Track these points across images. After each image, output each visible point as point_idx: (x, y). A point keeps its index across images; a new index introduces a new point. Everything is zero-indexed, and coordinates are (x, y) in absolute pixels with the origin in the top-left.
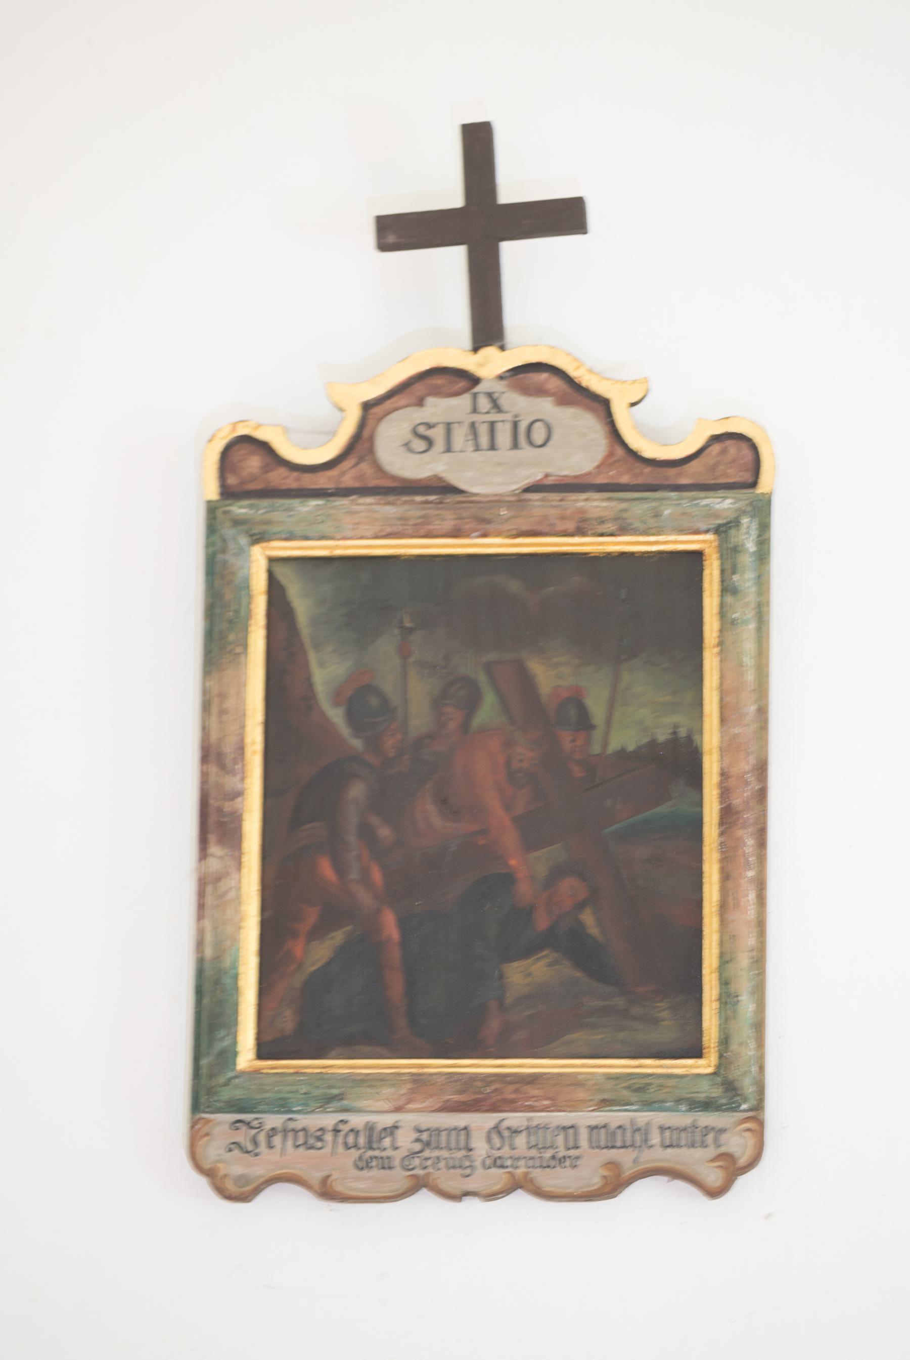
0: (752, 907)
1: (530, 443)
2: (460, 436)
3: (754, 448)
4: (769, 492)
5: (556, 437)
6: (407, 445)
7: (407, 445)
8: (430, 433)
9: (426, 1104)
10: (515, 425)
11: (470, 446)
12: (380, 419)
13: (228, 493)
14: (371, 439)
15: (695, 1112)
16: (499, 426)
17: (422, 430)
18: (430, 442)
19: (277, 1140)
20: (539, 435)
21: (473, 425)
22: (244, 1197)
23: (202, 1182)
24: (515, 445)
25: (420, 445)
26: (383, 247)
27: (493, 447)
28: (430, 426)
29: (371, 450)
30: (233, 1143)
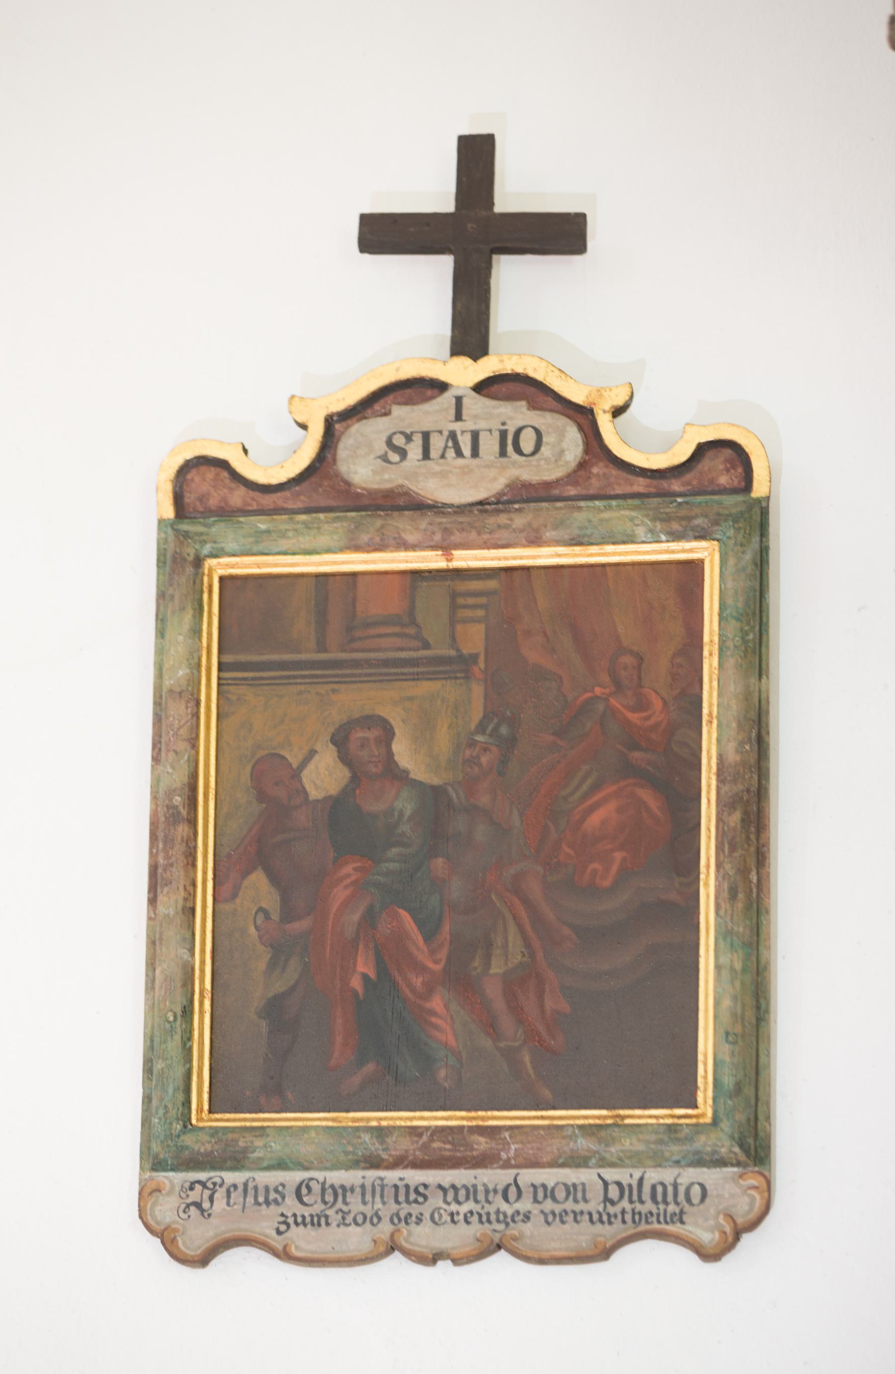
1: (518, 450)
2: (437, 443)
7: (385, 458)
11: (451, 453)
16: (483, 438)
20: (527, 442)
21: (453, 436)
22: (203, 1260)
24: (503, 453)
27: (475, 453)
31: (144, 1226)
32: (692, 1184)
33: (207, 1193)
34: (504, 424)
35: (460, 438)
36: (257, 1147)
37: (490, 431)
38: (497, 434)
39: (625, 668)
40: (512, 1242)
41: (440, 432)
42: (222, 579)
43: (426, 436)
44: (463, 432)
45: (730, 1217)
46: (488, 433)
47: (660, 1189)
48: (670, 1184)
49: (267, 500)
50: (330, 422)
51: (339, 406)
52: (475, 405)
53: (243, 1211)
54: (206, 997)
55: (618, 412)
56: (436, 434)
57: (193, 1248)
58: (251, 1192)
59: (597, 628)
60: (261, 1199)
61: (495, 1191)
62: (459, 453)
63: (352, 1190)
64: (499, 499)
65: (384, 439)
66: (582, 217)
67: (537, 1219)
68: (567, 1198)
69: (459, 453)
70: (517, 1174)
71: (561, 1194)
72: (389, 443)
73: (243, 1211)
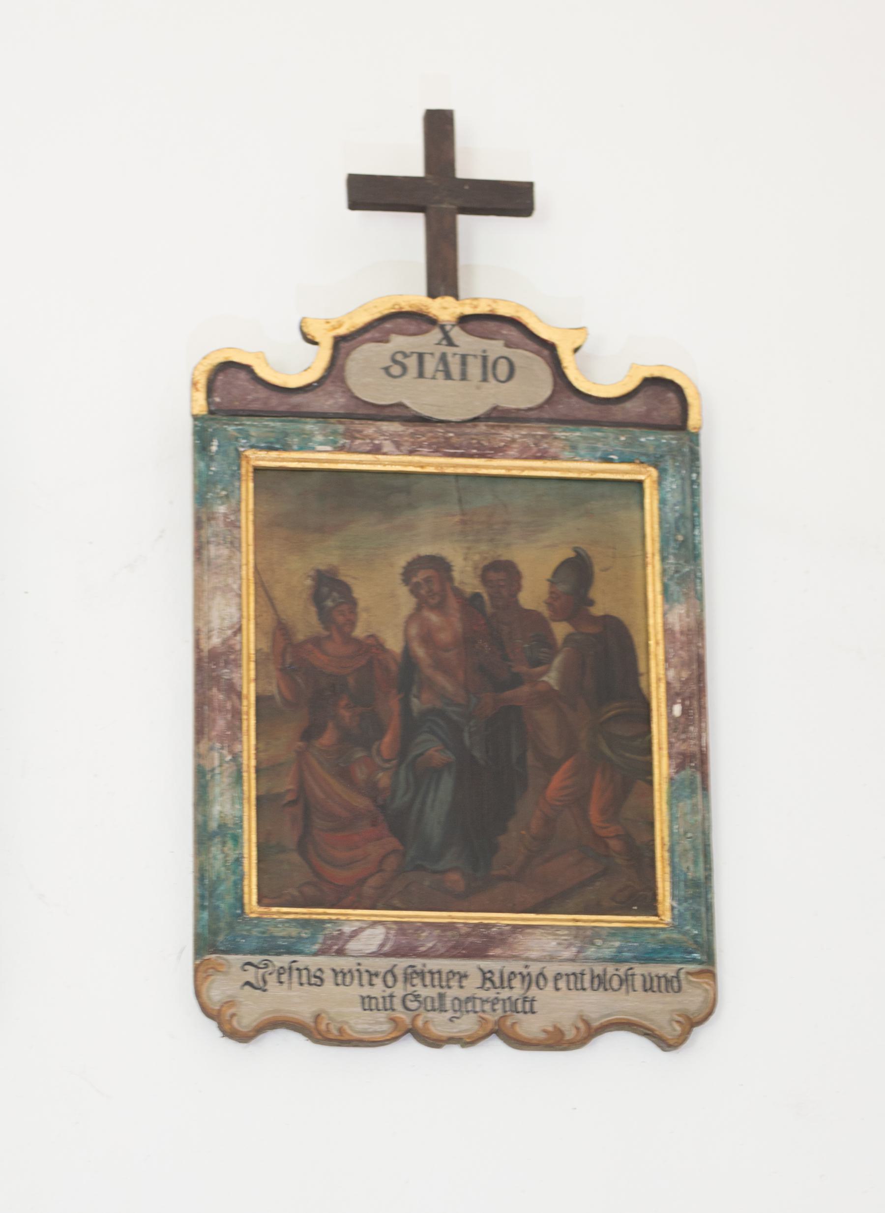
0: (665, 784)
1: (495, 376)
2: (430, 365)
3: (678, 390)
4: (698, 426)
5: (518, 372)
6: (387, 369)
7: (387, 369)
8: (406, 361)
9: (417, 952)
10: (485, 359)
11: (440, 375)
12: (348, 354)
13: (213, 412)
14: (342, 369)
15: (581, 962)
16: (470, 360)
17: (399, 357)
18: (404, 368)
19: (562, 984)
21: (443, 358)
23: (212, 1025)
25: (396, 370)
26: (354, 204)
27: (464, 377)
28: (405, 355)
29: (342, 380)
30: (541, 989)
32: (428, 997)
34: (484, 351)
35: (450, 359)
36: (671, 609)
41: (432, 354)
45: (586, 1022)
48: (393, 992)
50: (339, 341)
51: (343, 331)
52: (456, 334)
53: (316, 343)
54: (445, 993)
55: (576, 350)
56: (430, 356)
57: (246, 1020)
59: (464, 952)
60: (436, 976)
62: (448, 376)
63: (376, 975)
71: (328, 975)
73: (316, 343)
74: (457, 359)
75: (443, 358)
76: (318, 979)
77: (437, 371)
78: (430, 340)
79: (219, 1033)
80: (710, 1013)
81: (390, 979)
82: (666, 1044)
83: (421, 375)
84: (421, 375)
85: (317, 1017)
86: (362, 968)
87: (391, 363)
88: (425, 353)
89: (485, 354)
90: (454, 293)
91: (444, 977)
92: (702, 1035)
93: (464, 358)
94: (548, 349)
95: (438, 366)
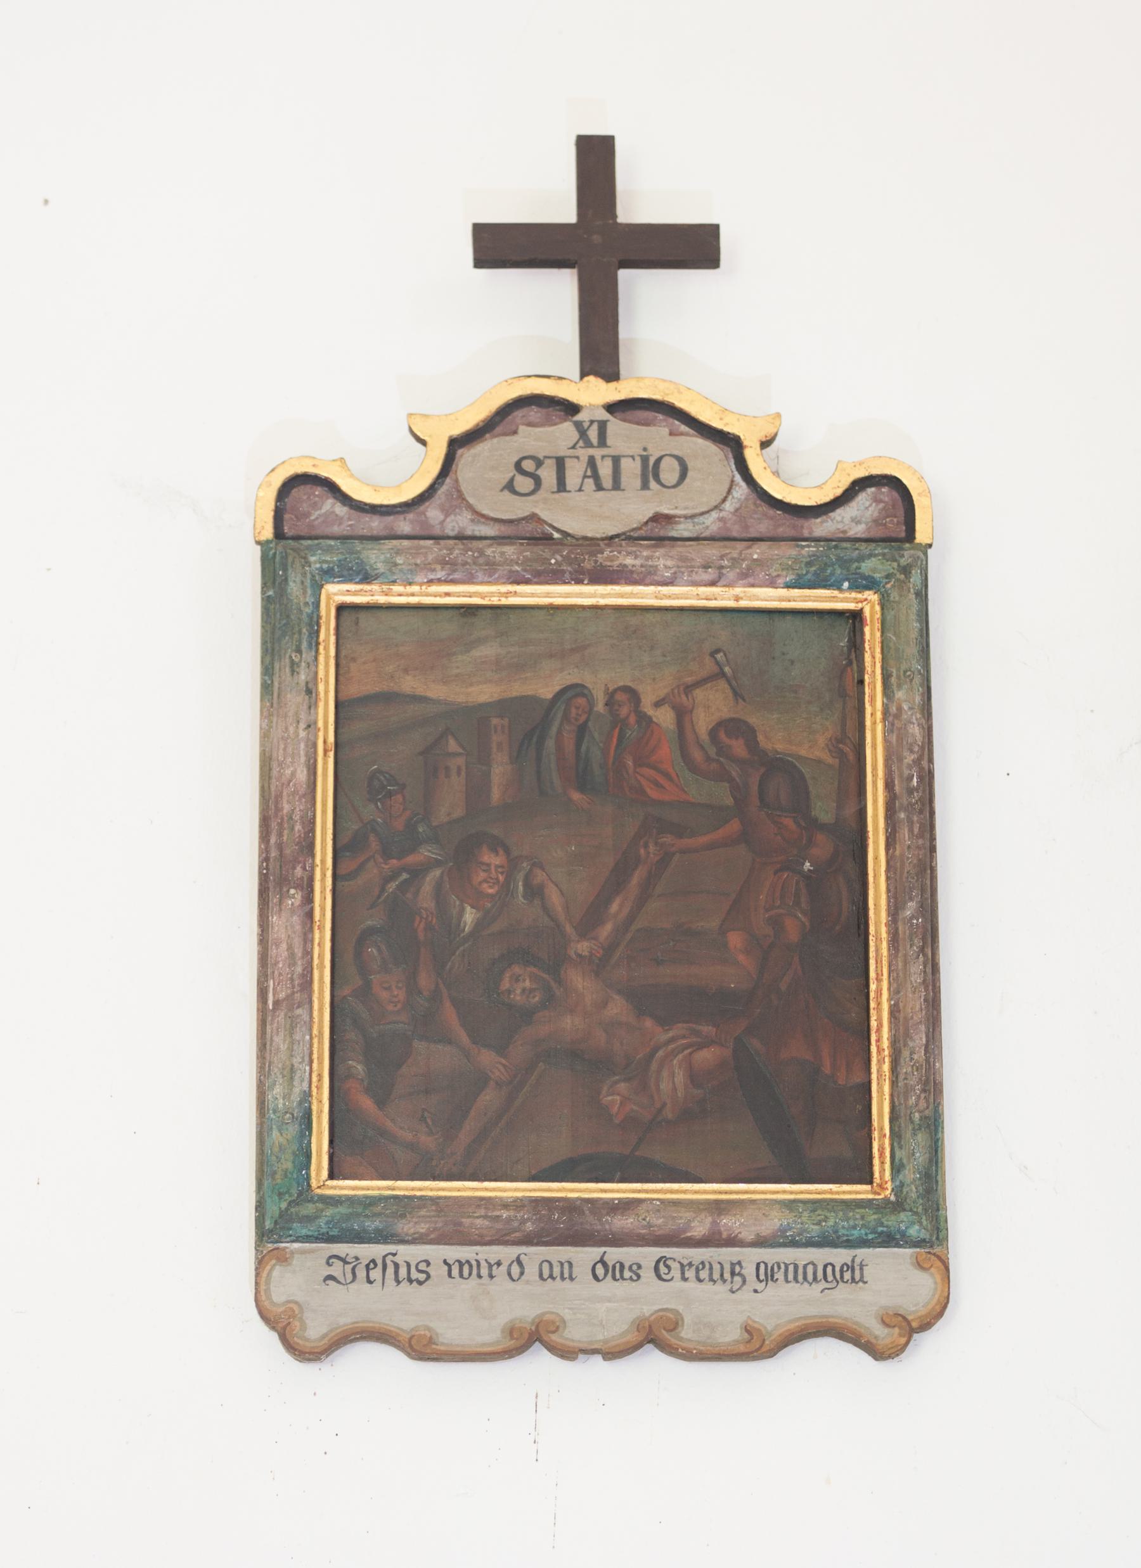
2: (575, 472)
6: (510, 487)
7: (510, 487)
11: (590, 482)
16: (625, 463)
17: (528, 465)
21: (592, 462)
24: (645, 486)
26: (712, 232)
27: (617, 486)
31: (685, 1360)
33: (349, 1268)
34: (645, 449)
35: (599, 462)
37: (633, 457)
38: (638, 459)
39: (577, 708)
40: (664, 1332)
42: (341, 609)
43: (560, 463)
44: (603, 457)
46: (631, 459)
47: (810, 1269)
49: (375, 524)
55: (765, 444)
57: (315, 1330)
58: (390, 1270)
61: (499, 1264)
64: (286, 510)
65: (516, 459)
66: (716, 228)
67: (648, 1274)
68: (606, 1275)
69: (599, 487)
70: (605, 1252)
72: (518, 466)
74: (608, 463)
75: (592, 462)
76: (419, 1276)
77: (585, 477)
78: (564, 433)
79: (870, 1359)
80: (941, 1314)
81: (515, 1269)
82: (878, 1353)
83: (562, 486)
84: (562, 486)
85: (748, 1330)
86: (398, 1259)
87: (539, 472)
88: (566, 457)
89: (645, 453)
90: (612, 375)
91: (837, 1269)
92: (927, 1344)
93: (616, 460)
94: (732, 444)
95: (586, 471)
